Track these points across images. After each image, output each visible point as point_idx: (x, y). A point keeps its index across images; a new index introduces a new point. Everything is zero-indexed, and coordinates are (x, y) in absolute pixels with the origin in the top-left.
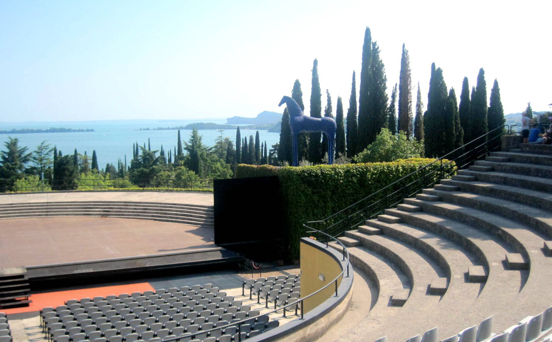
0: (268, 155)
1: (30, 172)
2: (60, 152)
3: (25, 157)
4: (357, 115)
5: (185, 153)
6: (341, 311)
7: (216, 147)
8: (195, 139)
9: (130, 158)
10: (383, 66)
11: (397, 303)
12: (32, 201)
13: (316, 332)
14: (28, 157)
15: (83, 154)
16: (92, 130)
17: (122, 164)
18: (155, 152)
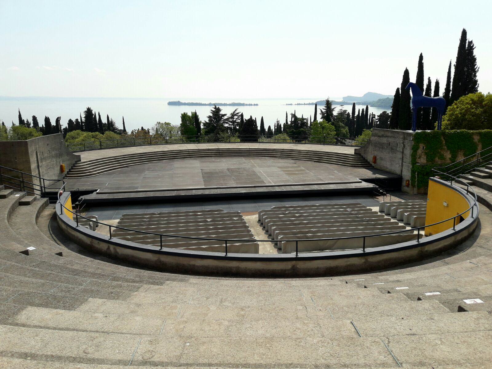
10: (475, 59)
13: (462, 238)
16: (257, 105)
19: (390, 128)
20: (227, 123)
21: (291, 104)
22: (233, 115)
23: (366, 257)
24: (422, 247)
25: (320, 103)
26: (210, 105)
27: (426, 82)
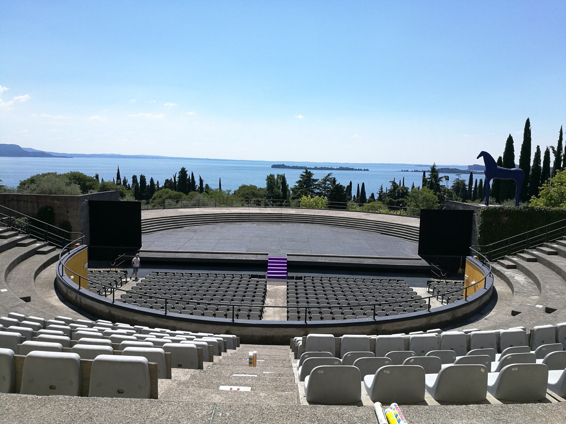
2: (152, 180)
16: (368, 170)
20: (318, 189)
21: (407, 171)
22: (325, 180)
23: (306, 329)
24: (378, 326)
25: (428, 171)
26: (301, 168)
27: (533, 151)
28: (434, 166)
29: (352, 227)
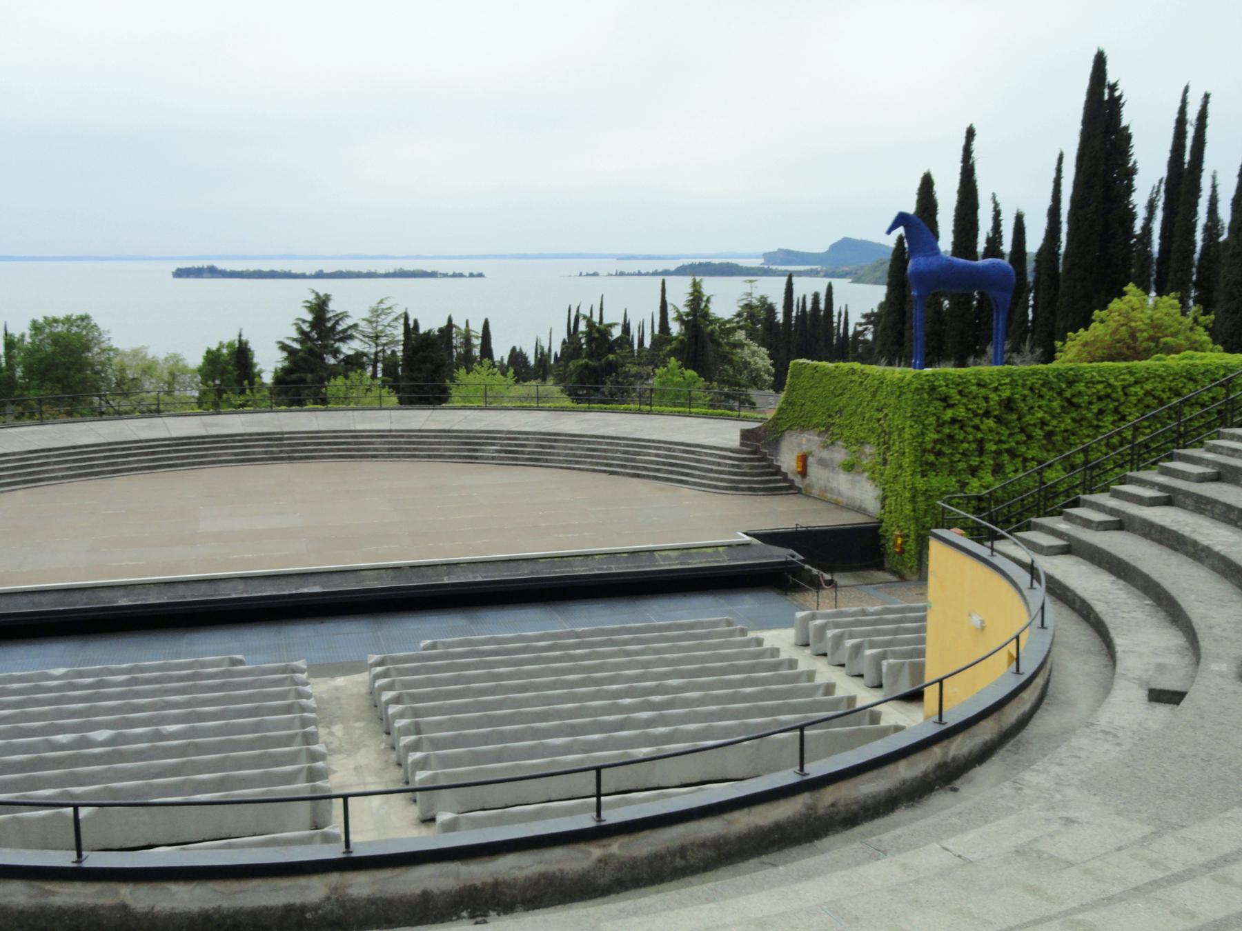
0: (851, 332)
1: (355, 362)
2: (416, 322)
3: (344, 331)
4: (1063, 250)
5: (675, 328)
6: (1027, 707)
7: (739, 315)
8: (697, 298)
9: (561, 334)
10: (1129, 137)
11: (1159, 696)
12: (359, 427)
14: (349, 332)
15: (463, 327)
16: (480, 275)
17: (542, 348)
18: (611, 325)
19: (807, 372)
24: (816, 794)
28: (34, 322)
29: (536, 460)
